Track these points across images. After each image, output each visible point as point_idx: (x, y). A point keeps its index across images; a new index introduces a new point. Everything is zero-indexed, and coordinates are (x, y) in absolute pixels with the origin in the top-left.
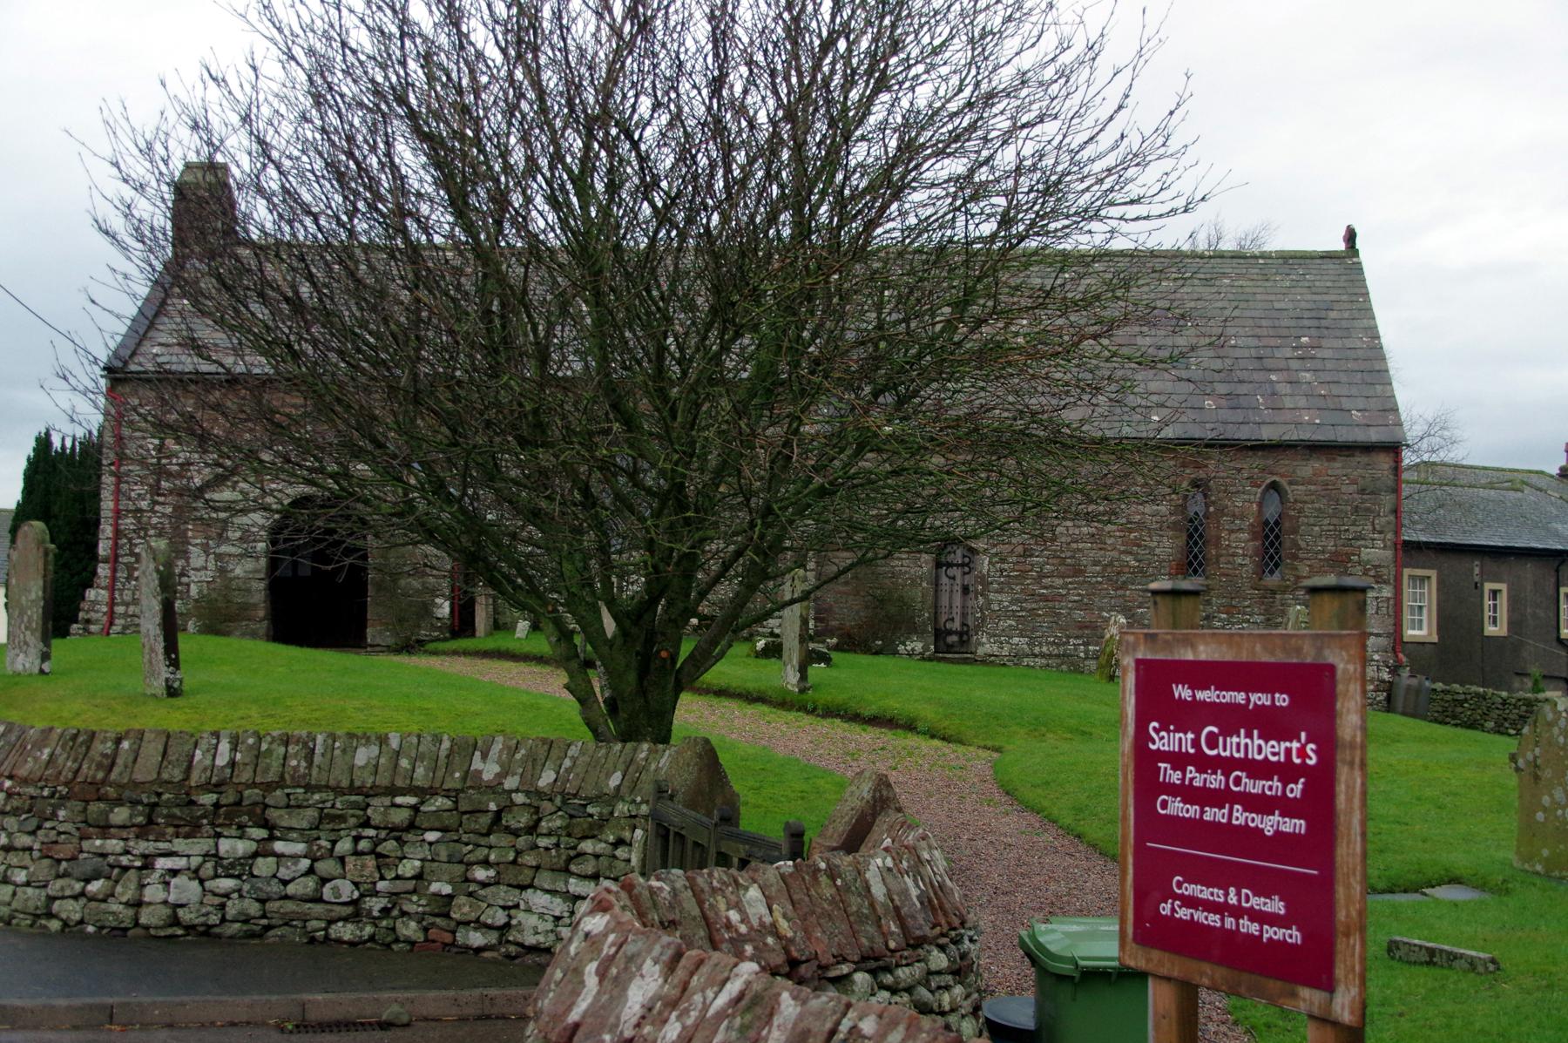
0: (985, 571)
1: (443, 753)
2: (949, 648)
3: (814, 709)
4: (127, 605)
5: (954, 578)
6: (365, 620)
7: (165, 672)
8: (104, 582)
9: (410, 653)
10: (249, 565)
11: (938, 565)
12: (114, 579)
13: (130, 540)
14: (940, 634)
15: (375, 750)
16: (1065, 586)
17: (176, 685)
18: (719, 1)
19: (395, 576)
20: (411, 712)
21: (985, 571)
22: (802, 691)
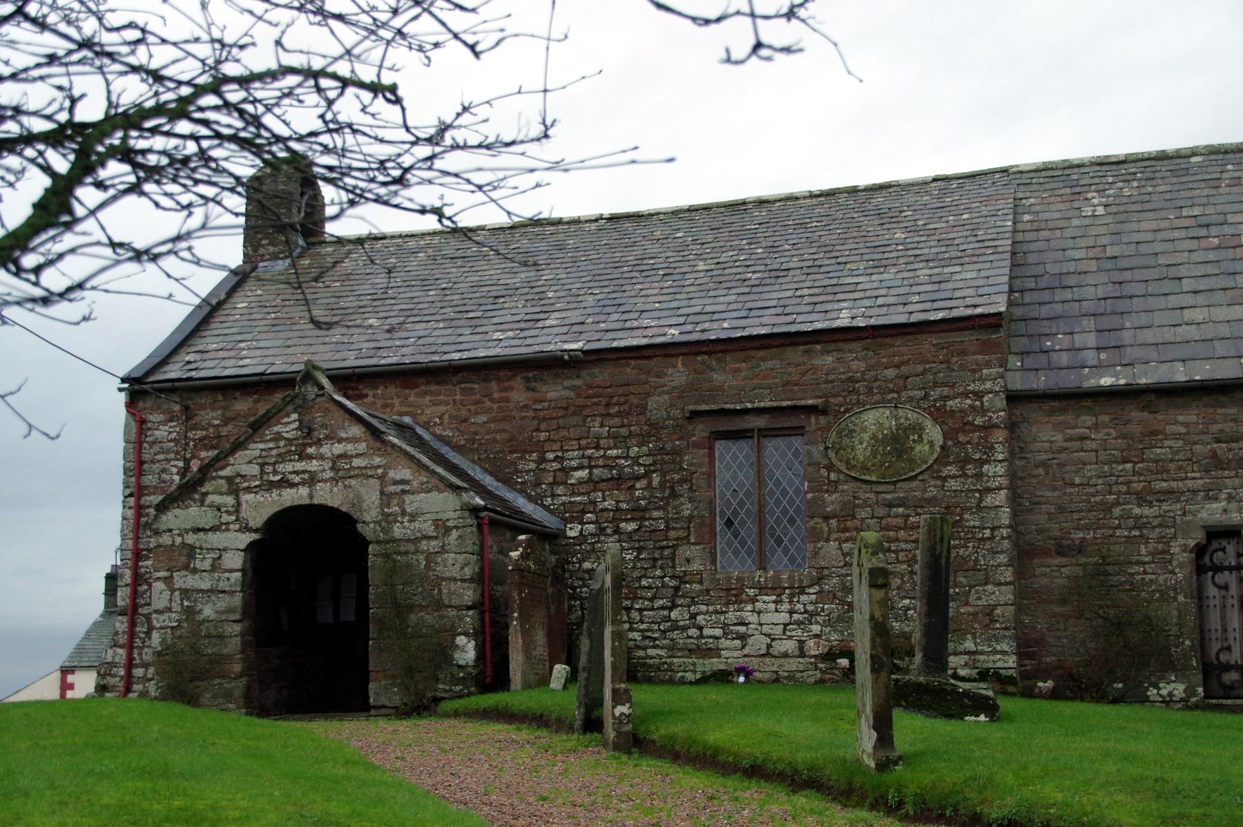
2: (1228, 691)
3: (900, 804)
5: (1226, 587)
10: (223, 603)
11: (1200, 570)
14: (1211, 671)
18: (1242, 692)
22: (884, 766)
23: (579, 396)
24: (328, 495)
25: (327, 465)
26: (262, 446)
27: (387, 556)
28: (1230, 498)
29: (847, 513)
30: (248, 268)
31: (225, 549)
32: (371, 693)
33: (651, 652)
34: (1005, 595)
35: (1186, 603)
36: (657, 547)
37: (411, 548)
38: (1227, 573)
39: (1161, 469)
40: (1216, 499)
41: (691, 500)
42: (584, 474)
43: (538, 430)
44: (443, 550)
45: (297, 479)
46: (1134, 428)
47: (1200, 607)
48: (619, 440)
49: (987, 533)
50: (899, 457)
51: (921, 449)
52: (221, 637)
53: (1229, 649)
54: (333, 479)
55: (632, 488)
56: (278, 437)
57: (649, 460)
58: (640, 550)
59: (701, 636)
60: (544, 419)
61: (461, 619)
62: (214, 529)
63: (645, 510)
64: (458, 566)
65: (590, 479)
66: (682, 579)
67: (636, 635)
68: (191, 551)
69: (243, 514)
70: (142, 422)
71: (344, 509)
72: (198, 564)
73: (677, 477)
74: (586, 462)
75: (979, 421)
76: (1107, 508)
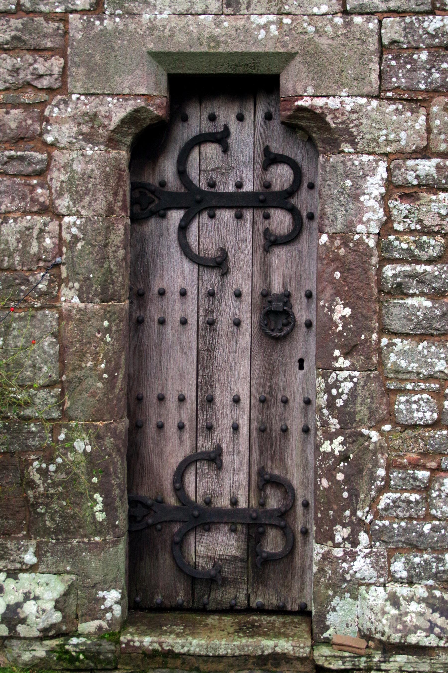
0: (367, 230)
5: (220, 264)
11: (145, 203)
21: (367, 230)
35: (84, 318)
38: (226, 215)
47: (137, 324)
53: (215, 458)
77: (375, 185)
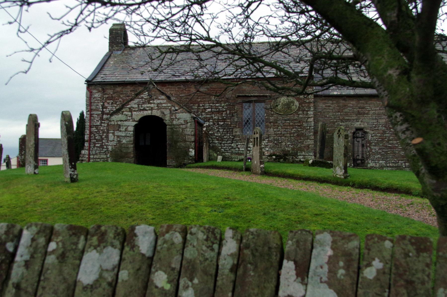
0: (370, 139)
1: (226, 263)
4: (94, 155)
5: (359, 142)
6: (167, 157)
7: (70, 171)
8: (87, 148)
9: (181, 168)
10: (128, 139)
11: (354, 138)
12: (90, 147)
13: (94, 135)
15: (112, 255)
16: (397, 143)
17: (75, 177)
19: (176, 142)
20: (181, 188)
21: (370, 139)
22: (346, 178)
23: (208, 90)
24: (156, 113)
25: (156, 105)
26: (138, 100)
27: (172, 129)
28: (361, 121)
29: (275, 122)
30: (110, 53)
31: (129, 126)
32: (168, 162)
33: (226, 154)
34: (312, 142)
36: (228, 129)
37: (178, 127)
39: (347, 114)
40: (358, 122)
41: (237, 117)
42: (210, 110)
43: (198, 98)
44: (186, 128)
45: (148, 109)
46: (341, 104)
48: (218, 102)
49: (308, 128)
50: (288, 109)
51: (294, 107)
52: (128, 148)
53: (359, 155)
54: (157, 109)
55: (222, 114)
56: (142, 98)
57: (227, 107)
58: (224, 129)
59: (239, 150)
60: (200, 96)
61: (191, 145)
62: (126, 121)
63: (225, 119)
64: (190, 132)
65: (211, 111)
66: (234, 136)
67: (223, 150)
68: (119, 126)
69: (133, 117)
70: (91, 92)
71: (160, 117)
72: (121, 129)
73: (233, 111)
74: (210, 107)
75: (307, 101)
76: (334, 123)
77: (370, 136)
